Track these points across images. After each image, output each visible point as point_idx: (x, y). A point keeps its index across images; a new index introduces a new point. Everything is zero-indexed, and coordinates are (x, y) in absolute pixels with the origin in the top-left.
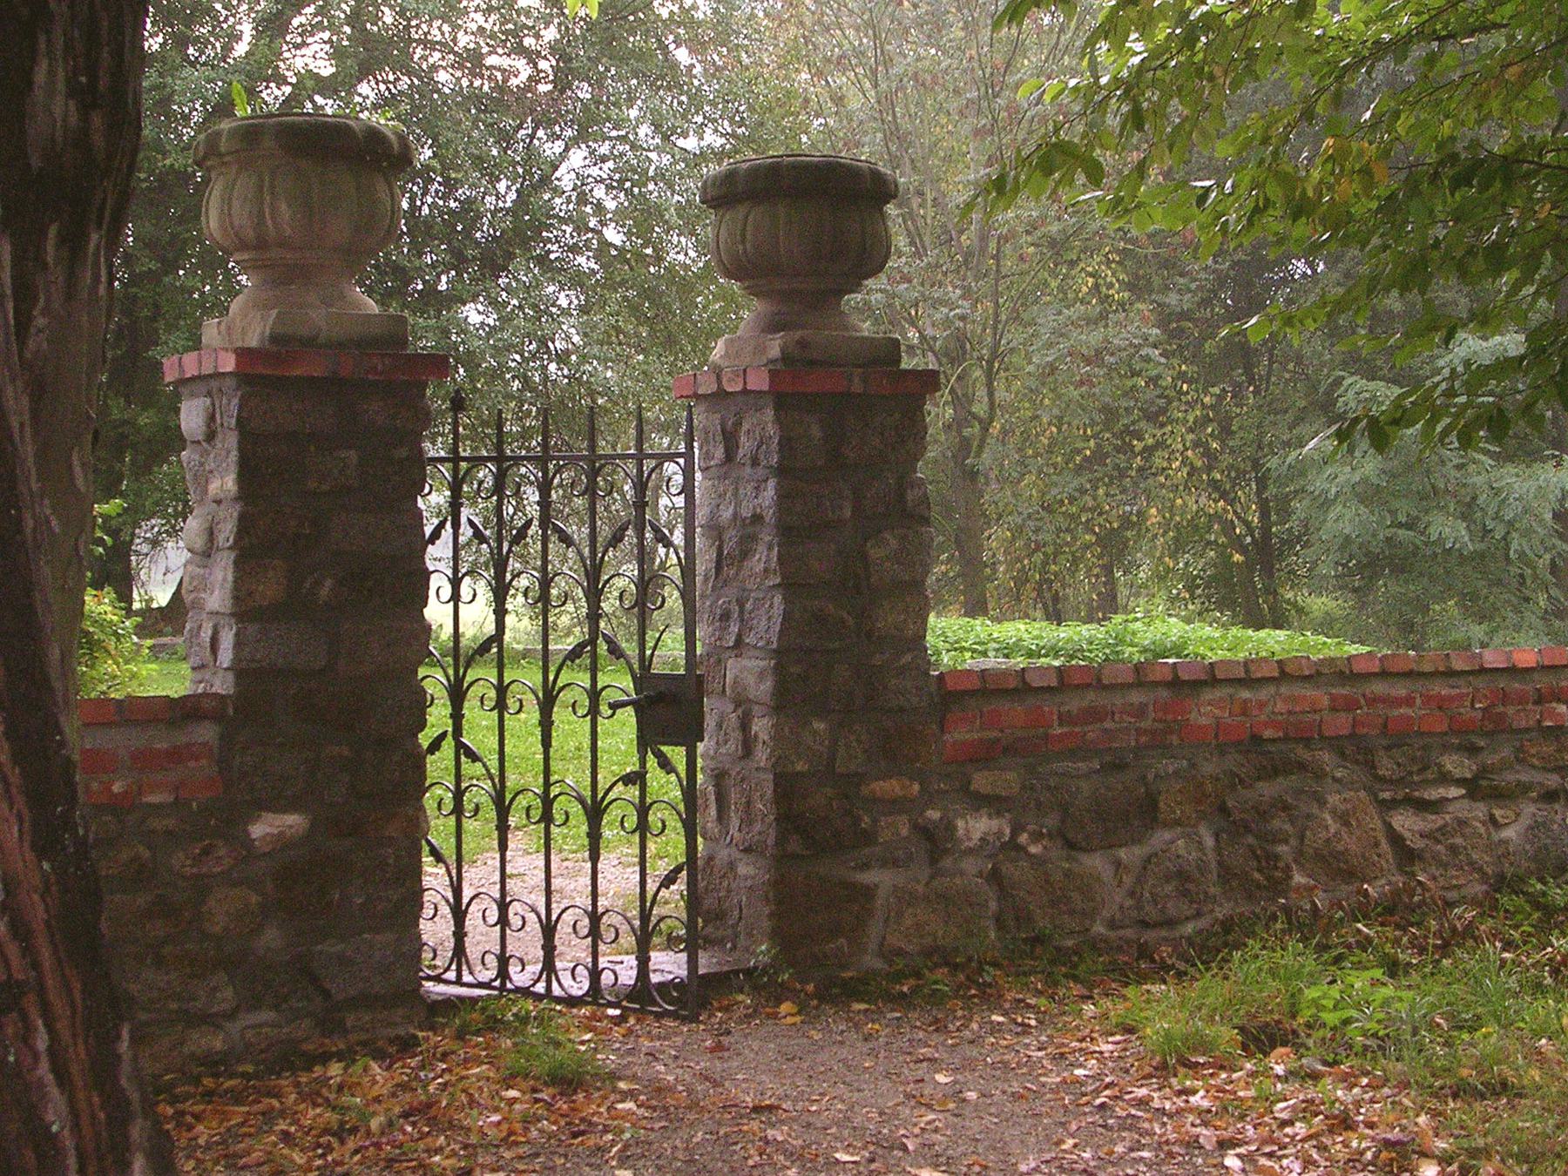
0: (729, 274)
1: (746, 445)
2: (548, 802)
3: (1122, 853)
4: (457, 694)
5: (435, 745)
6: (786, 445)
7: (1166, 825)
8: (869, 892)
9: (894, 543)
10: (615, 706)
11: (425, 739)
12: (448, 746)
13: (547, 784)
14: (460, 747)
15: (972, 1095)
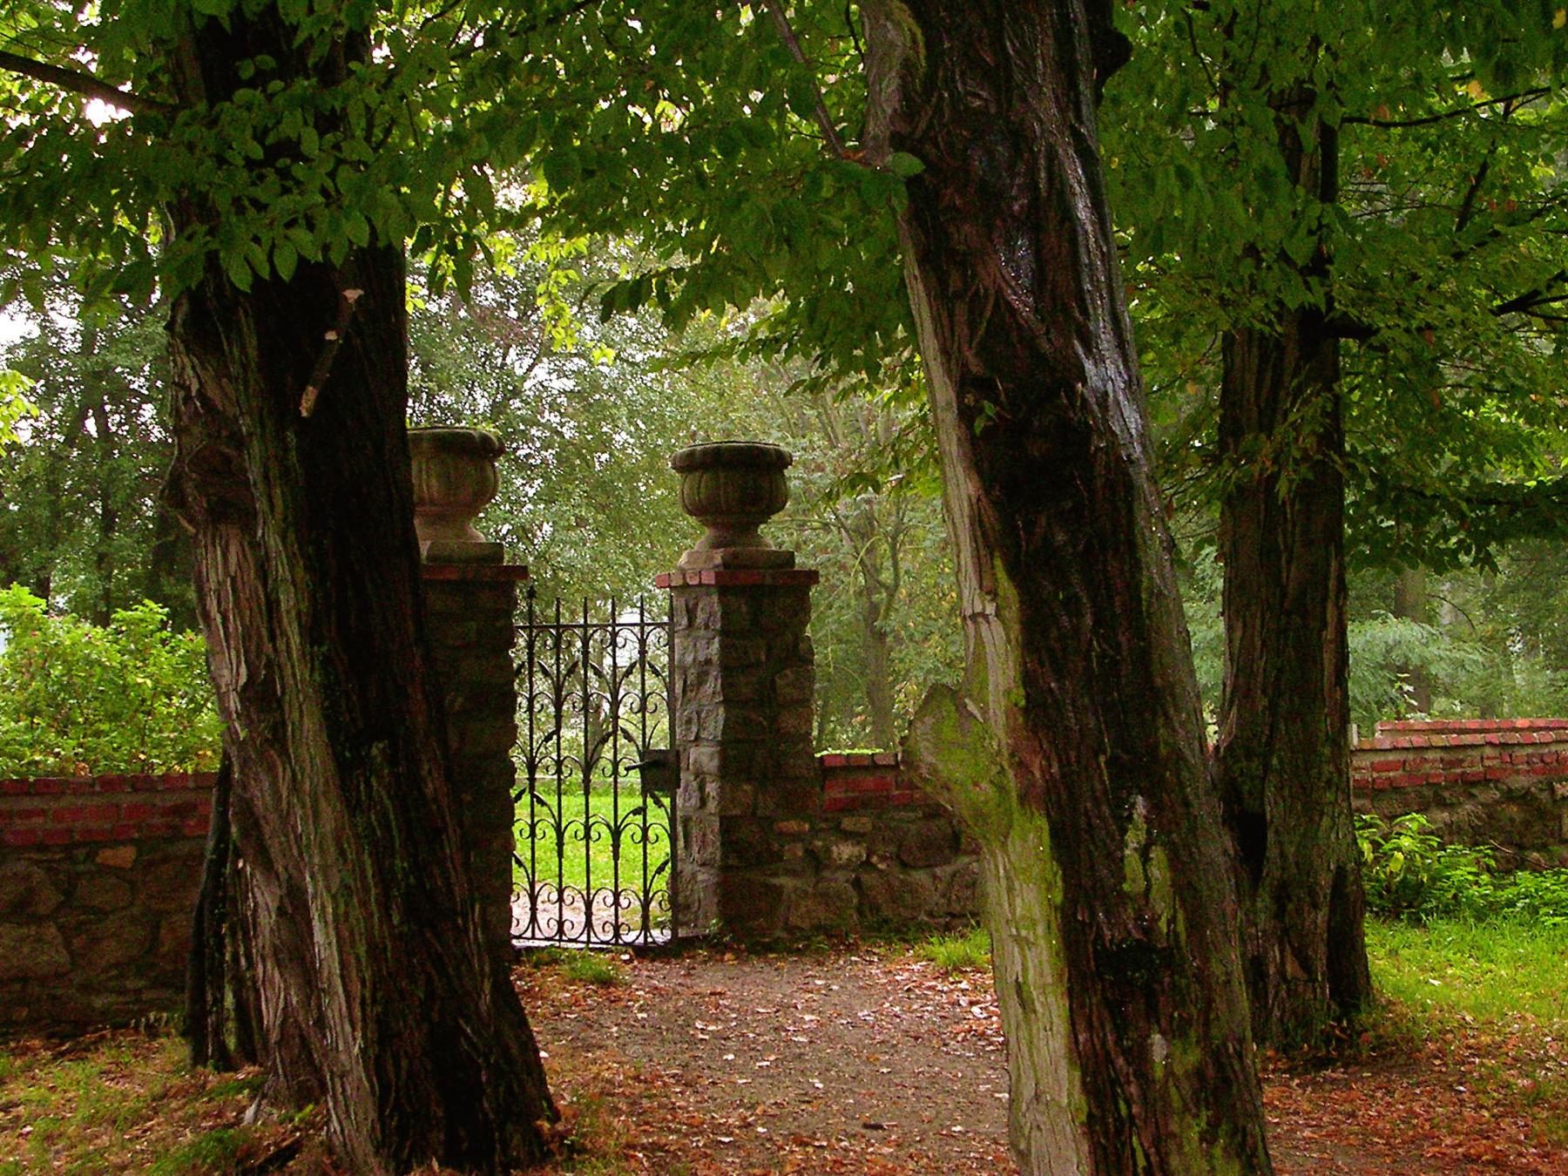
0: (691, 513)
1: (701, 617)
2: (588, 828)
3: (938, 871)
4: (532, 767)
5: (519, 797)
6: (725, 616)
7: (966, 853)
8: (778, 890)
9: (792, 677)
10: (628, 769)
11: (513, 793)
12: (526, 798)
13: (587, 818)
14: (533, 796)
15: (835, 987)
